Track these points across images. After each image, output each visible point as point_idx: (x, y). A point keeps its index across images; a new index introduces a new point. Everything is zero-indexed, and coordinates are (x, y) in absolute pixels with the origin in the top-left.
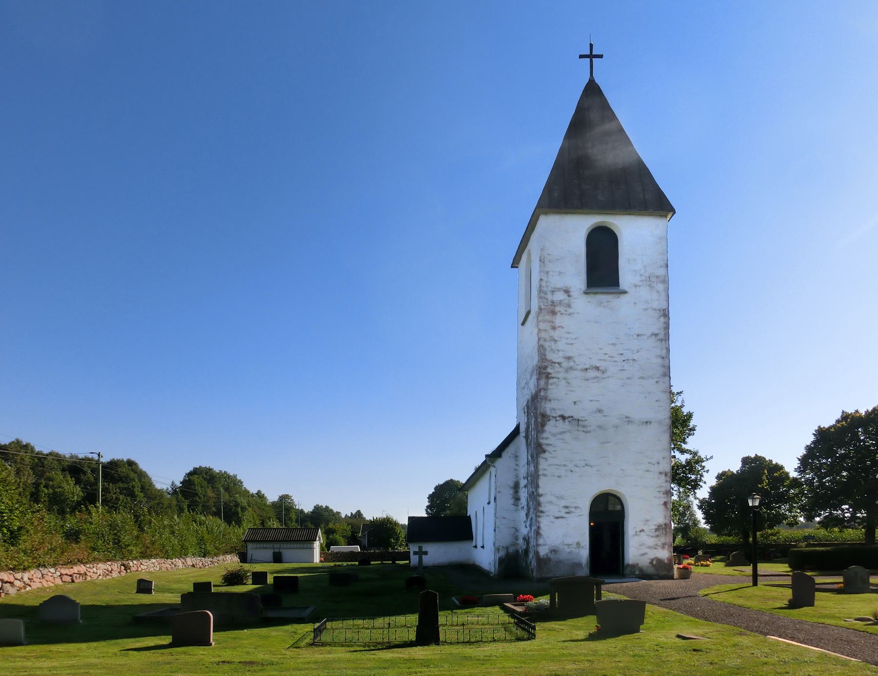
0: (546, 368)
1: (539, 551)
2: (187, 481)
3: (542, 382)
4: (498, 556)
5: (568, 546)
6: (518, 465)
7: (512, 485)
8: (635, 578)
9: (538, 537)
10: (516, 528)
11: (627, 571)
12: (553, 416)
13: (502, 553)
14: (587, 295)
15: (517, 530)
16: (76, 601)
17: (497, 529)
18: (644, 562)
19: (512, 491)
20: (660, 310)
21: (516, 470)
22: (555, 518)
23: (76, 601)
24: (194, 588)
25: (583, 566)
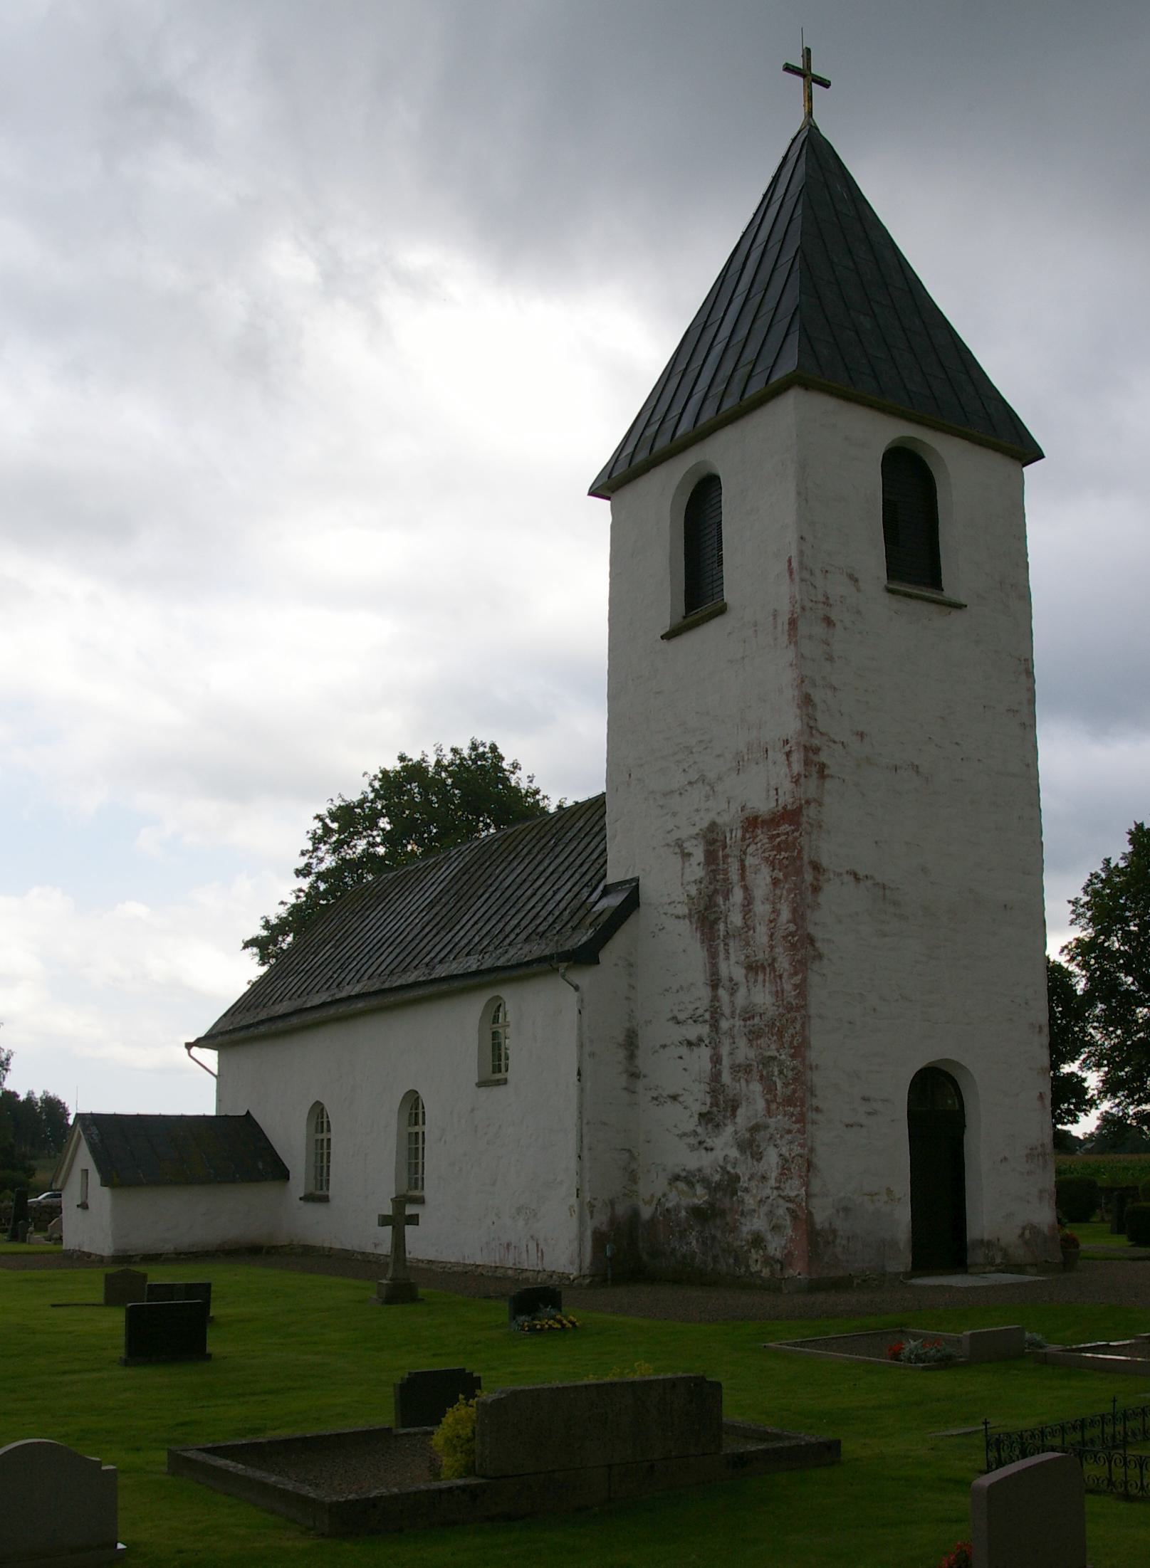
0: (817, 750)
1: (814, 1211)
2: (1062, 970)
3: (811, 787)
4: (590, 1225)
5: (869, 1197)
6: (634, 988)
7: (621, 1038)
8: (994, 1272)
9: (810, 1174)
10: (629, 1151)
11: (975, 1256)
12: (834, 872)
13: (601, 1219)
14: (890, 595)
15: (633, 1157)
16: (464, 1370)
17: (586, 1154)
18: (1009, 1235)
19: (622, 1054)
20: (1019, 660)
21: (628, 998)
22: (847, 1126)
23: (464, 1370)
24: (205, 1340)
25: (901, 1246)
